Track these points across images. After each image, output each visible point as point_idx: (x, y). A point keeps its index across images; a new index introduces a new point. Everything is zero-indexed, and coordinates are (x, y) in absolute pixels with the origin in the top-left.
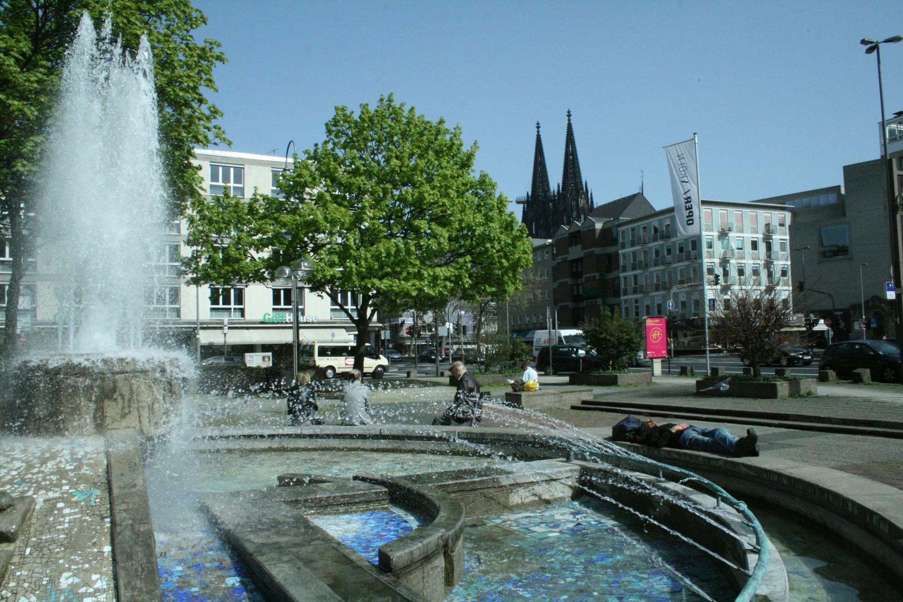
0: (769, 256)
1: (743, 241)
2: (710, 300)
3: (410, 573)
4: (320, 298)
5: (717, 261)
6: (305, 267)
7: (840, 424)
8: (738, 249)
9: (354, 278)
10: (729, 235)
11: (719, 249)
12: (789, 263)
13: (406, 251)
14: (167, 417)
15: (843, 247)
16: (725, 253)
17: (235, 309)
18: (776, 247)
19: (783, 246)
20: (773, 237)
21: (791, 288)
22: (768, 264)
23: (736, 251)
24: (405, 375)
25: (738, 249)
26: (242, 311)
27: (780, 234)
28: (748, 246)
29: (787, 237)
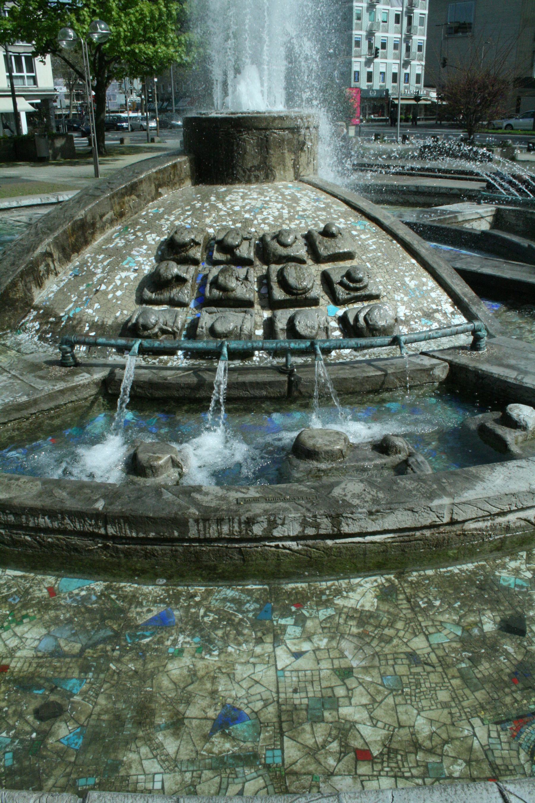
0: (409, 30)
1: (388, 14)
2: (355, 72)
3: (249, 373)
4: (42, 64)
5: (364, 33)
6: (101, 29)
7: (145, 147)
8: (383, 22)
9: (121, 43)
10: (377, 7)
11: (366, 21)
12: (425, 38)
13: (167, 15)
14: (480, 331)
15: (464, 24)
16: (372, 25)
17: (28, 77)
18: (416, 22)
19: (422, 20)
20: (415, 11)
21: (423, 63)
22: (408, 38)
23: (382, 24)
24: (119, 142)
25: (383, 22)
26: (34, 79)
27: (421, 9)
28: (392, 19)
29: (426, 12)
